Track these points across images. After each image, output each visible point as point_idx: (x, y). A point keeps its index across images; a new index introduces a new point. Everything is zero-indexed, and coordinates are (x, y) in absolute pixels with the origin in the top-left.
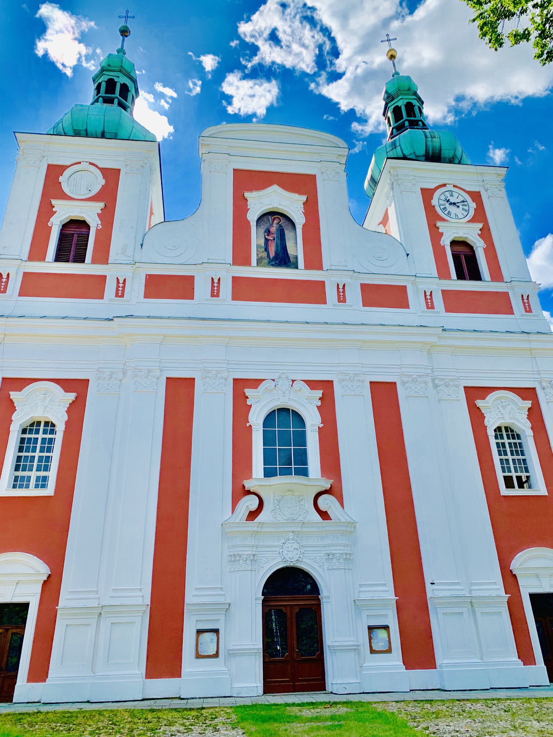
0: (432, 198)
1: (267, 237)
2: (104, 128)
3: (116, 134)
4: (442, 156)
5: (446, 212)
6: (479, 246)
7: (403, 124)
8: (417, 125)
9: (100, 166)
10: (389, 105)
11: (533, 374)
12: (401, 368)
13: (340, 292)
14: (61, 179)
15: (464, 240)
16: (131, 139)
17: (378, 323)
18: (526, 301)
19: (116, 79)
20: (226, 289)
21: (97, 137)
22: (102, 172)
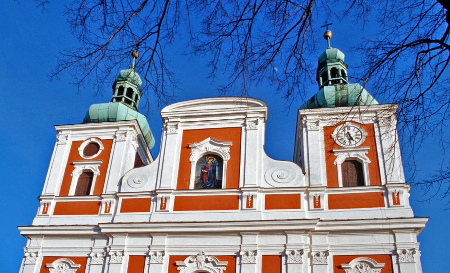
0: (79, 147)
1: (203, 170)
2: (108, 116)
3: (116, 119)
4: (349, 102)
5: (342, 142)
6: (366, 162)
7: (121, 98)
8: (339, 82)
9: (102, 139)
10: (319, 72)
11: (390, 245)
12: (382, 246)
13: (249, 201)
14: (79, 149)
15: (355, 159)
16: (126, 120)
17: (373, 218)
18: (396, 197)
19: (337, 67)
20: (325, 203)
21: (105, 122)
22: (102, 142)
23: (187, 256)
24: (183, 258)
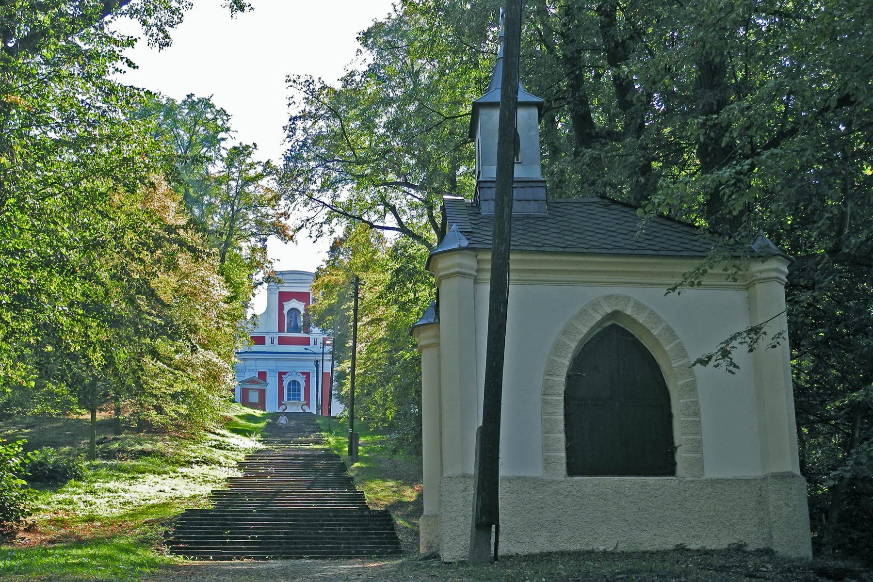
20: (276, 341)
23: (287, 372)
24: (285, 373)
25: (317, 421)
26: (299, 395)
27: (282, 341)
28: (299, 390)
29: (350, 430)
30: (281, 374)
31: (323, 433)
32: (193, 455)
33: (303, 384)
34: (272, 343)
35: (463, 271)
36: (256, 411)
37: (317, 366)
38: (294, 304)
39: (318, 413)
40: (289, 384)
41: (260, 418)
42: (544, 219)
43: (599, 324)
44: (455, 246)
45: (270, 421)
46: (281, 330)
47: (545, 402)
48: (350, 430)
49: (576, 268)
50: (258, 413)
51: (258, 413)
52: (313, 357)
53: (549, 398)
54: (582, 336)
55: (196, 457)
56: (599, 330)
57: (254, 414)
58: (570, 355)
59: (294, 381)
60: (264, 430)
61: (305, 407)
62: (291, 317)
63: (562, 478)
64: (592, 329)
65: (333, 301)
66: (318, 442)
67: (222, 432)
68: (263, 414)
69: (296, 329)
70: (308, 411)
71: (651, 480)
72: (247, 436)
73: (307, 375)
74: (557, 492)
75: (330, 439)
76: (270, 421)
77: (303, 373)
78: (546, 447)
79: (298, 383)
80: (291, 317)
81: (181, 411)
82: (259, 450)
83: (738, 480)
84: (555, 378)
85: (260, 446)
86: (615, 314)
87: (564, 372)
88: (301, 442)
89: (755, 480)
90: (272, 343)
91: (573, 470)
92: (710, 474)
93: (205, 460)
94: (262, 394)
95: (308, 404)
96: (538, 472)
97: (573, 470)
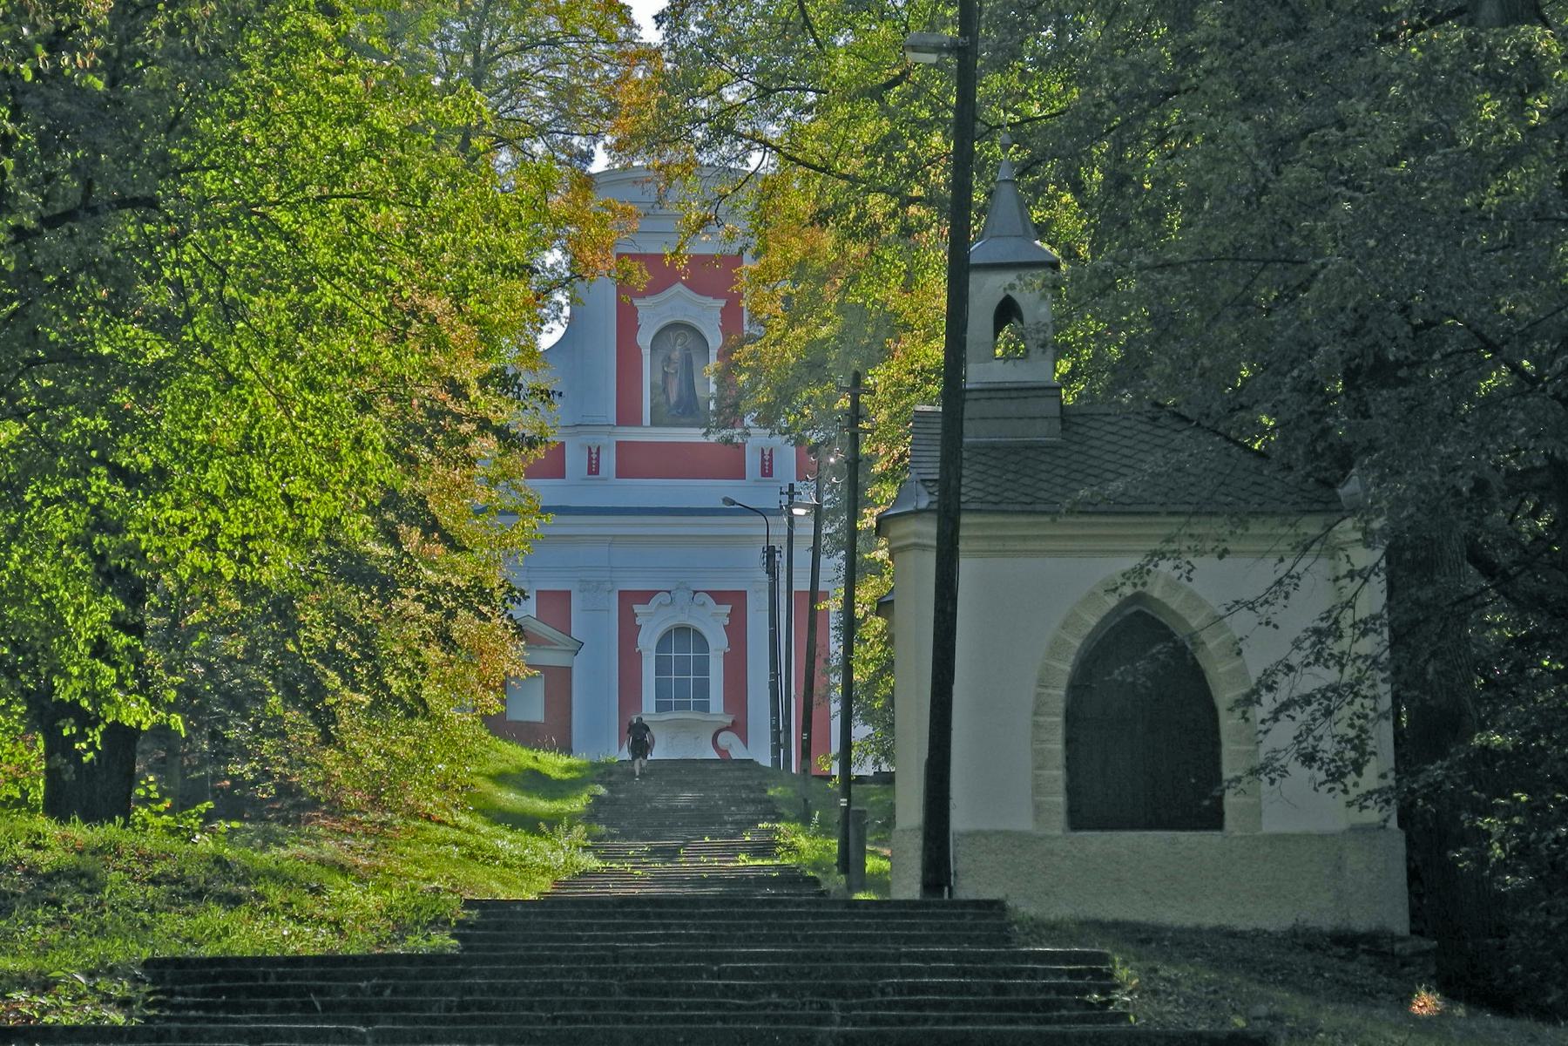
20: (609, 461)
24: (646, 596)
25: (771, 793)
26: (703, 689)
27: (633, 462)
28: (703, 667)
29: (843, 802)
30: (628, 599)
31: (781, 826)
32: (421, 873)
33: (718, 643)
34: (594, 469)
35: (920, 541)
36: (541, 755)
37: (771, 570)
38: (680, 303)
39: (776, 761)
40: (664, 643)
41: (560, 781)
42: (1055, 447)
43: (1116, 611)
44: (910, 508)
45: (602, 791)
46: (628, 414)
47: (1037, 726)
48: (843, 802)
49: (1081, 532)
50: (553, 764)
51: (553, 764)
52: (754, 527)
53: (1041, 719)
54: (1090, 629)
55: (429, 879)
56: (1118, 619)
57: (535, 765)
58: (1072, 658)
59: (683, 630)
60: (590, 817)
61: (726, 739)
62: (668, 360)
63: (1058, 832)
64: (1105, 620)
65: (824, 331)
66: (764, 849)
67: (464, 820)
68: (569, 769)
69: (687, 410)
70: (738, 753)
71: (1183, 836)
72: (541, 834)
73: (736, 600)
74: (1052, 853)
75: (802, 842)
76: (602, 791)
77: (719, 597)
78: (1037, 789)
79: (699, 636)
80: (668, 360)
81: (399, 750)
82: (584, 874)
83: (1308, 836)
84: (1050, 691)
85: (591, 862)
86: (1138, 598)
87: (1063, 681)
88: (709, 851)
89: (1333, 835)
90: (594, 469)
91: (1078, 819)
92: (1270, 826)
93: (454, 885)
94: (558, 682)
95: (739, 728)
96: (1024, 823)
97: (1078, 819)
